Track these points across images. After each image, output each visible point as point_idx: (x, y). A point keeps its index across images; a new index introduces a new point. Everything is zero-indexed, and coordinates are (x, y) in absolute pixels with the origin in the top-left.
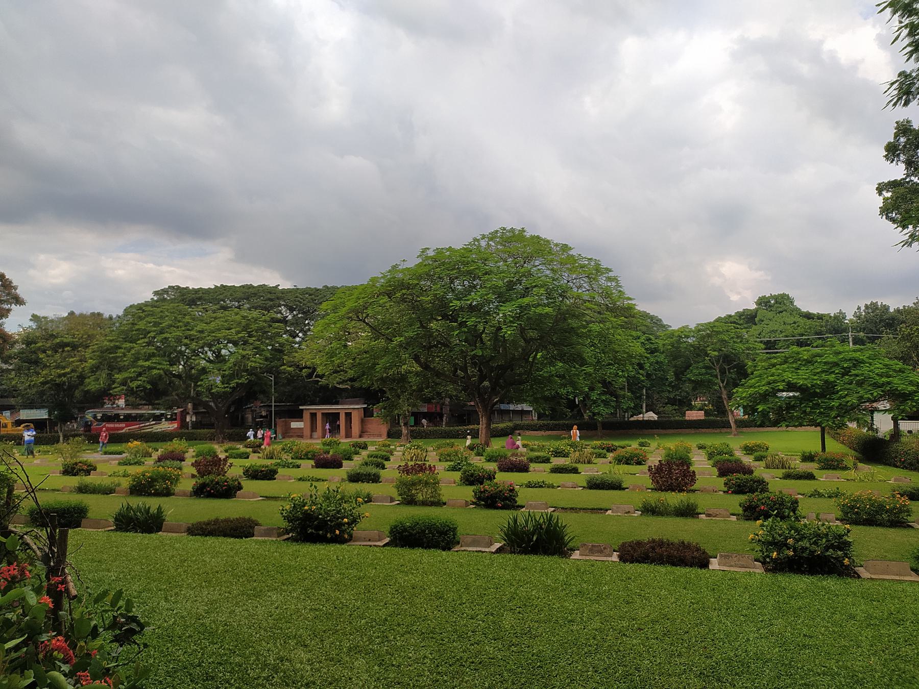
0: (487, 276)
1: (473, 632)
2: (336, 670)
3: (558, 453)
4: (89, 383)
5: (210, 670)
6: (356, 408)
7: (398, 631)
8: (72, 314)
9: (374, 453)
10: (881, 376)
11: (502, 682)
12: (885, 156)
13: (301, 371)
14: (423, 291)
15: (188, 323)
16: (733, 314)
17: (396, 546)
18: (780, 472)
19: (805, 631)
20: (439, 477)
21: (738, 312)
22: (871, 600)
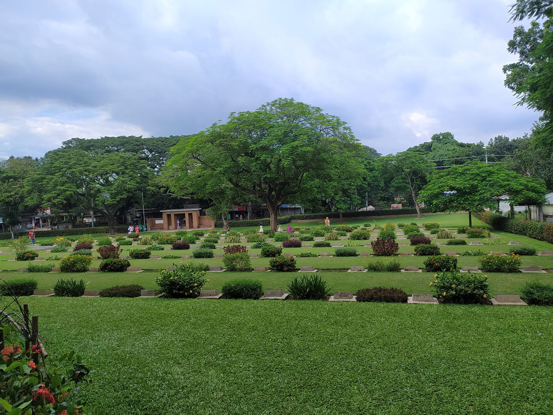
0: (272, 129)
1: (276, 350)
2: (199, 378)
3: (318, 234)
4: (27, 202)
5: (125, 383)
6: (195, 211)
7: (233, 351)
8: (12, 157)
9: (208, 239)
10: (504, 180)
11: (294, 379)
12: (508, 49)
13: (160, 188)
14: (233, 139)
15: (86, 161)
16: (418, 146)
17: (227, 298)
18: (446, 241)
19: (463, 339)
20: (249, 253)
21: (421, 144)
22: (498, 318)
